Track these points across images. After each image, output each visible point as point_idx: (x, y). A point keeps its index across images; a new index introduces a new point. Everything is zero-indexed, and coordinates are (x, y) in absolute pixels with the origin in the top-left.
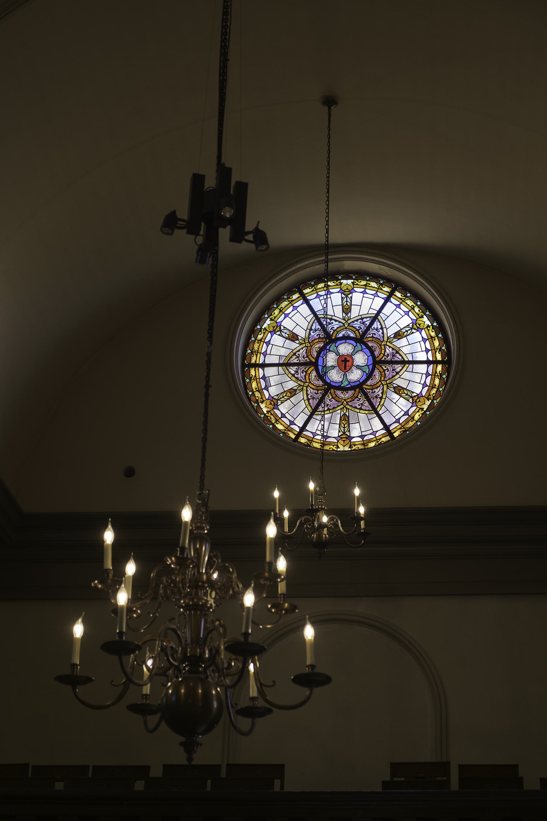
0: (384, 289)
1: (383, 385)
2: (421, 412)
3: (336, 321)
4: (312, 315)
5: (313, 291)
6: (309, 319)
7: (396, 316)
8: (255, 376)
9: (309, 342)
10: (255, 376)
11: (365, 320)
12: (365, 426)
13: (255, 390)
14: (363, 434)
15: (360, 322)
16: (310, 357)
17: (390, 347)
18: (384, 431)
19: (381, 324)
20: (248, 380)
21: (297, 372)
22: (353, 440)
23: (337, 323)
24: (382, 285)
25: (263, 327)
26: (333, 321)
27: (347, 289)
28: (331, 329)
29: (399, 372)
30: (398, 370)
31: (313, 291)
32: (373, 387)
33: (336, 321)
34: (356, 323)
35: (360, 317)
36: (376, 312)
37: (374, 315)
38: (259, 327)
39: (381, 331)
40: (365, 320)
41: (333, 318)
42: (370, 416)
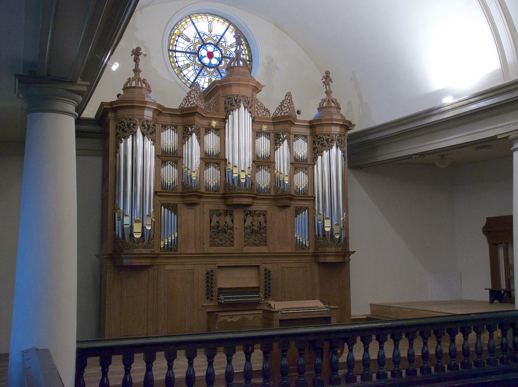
0: (171, 55)
1: (209, 74)
2: (214, 18)
3: (195, 68)
4: (198, 78)
5: (233, 29)
6: (200, 79)
7: (180, 45)
8: (187, 22)
9: (211, 37)
10: (187, 22)
11: (231, 55)
12: (189, 75)
13: (181, 24)
14: (186, 76)
15: (229, 54)
16: (215, 71)
17: (195, 41)
18: (191, 83)
19: (187, 49)
20: (184, 20)
21: (223, 73)
22: (181, 73)
23: (195, 67)
24: (248, 55)
25: (208, 17)
26: (195, 69)
27: (179, 70)
28: (199, 68)
29: (218, 77)
30: (218, 77)
31: (233, 29)
32: (206, 70)
33: (195, 68)
34: (229, 52)
35: (188, 59)
36: (182, 53)
37: (184, 54)
38: (207, 15)
39: (190, 48)
40: (231, 55)
41: (194, 69)
42: (194, 75)
